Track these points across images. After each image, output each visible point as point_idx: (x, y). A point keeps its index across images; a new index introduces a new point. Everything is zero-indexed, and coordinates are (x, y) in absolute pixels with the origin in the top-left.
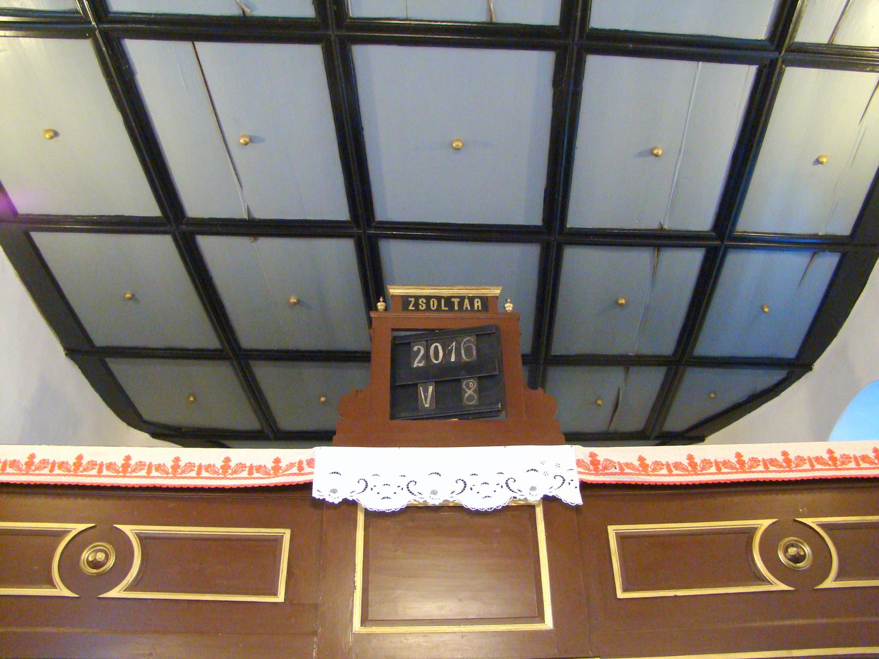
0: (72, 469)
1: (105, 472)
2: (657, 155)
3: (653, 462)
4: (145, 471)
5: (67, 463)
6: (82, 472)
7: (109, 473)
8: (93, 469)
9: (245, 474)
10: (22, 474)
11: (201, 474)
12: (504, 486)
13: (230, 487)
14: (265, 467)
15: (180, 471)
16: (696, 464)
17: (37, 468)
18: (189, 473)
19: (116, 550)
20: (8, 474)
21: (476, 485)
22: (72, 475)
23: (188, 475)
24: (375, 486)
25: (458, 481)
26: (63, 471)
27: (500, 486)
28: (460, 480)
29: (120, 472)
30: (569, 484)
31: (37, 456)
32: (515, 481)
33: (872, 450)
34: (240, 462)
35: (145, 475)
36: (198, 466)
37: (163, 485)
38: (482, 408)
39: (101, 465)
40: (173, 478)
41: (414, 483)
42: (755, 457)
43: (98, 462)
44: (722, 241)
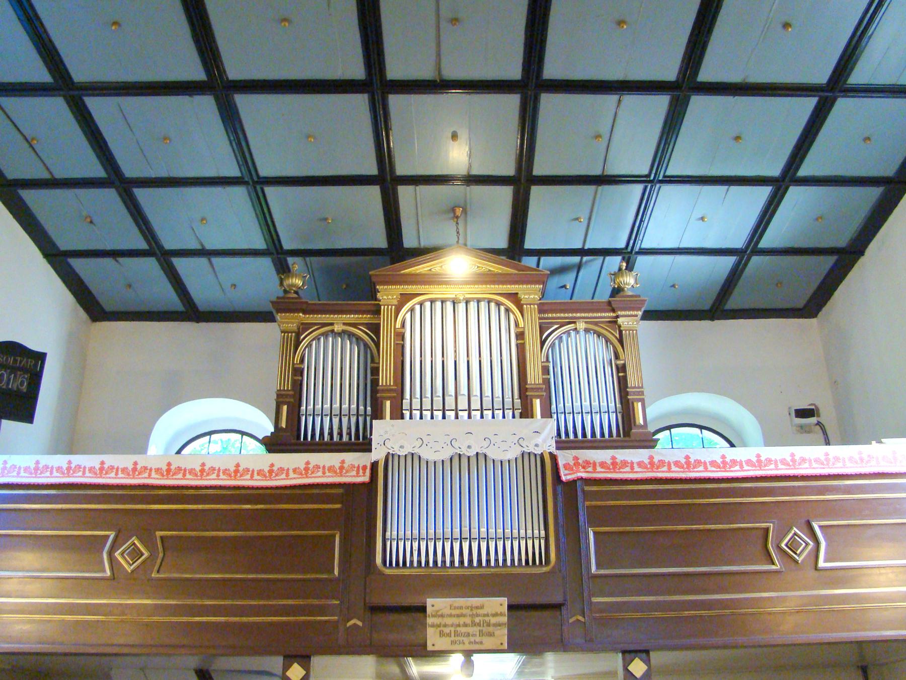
1: (188, 476)
2: (580, 222)
3: (583, 461)
5: (127, 468)
10: (198, 479)
15: (39, 472)
22: (304, 478)
23: (244, 478)
31: (206, 464)
33: (789, 455)
34: (281, 466)
35: (285, 477)
39: (151, 470)
42: (735, 459)
43: (286, 468)
44: (161, 256)
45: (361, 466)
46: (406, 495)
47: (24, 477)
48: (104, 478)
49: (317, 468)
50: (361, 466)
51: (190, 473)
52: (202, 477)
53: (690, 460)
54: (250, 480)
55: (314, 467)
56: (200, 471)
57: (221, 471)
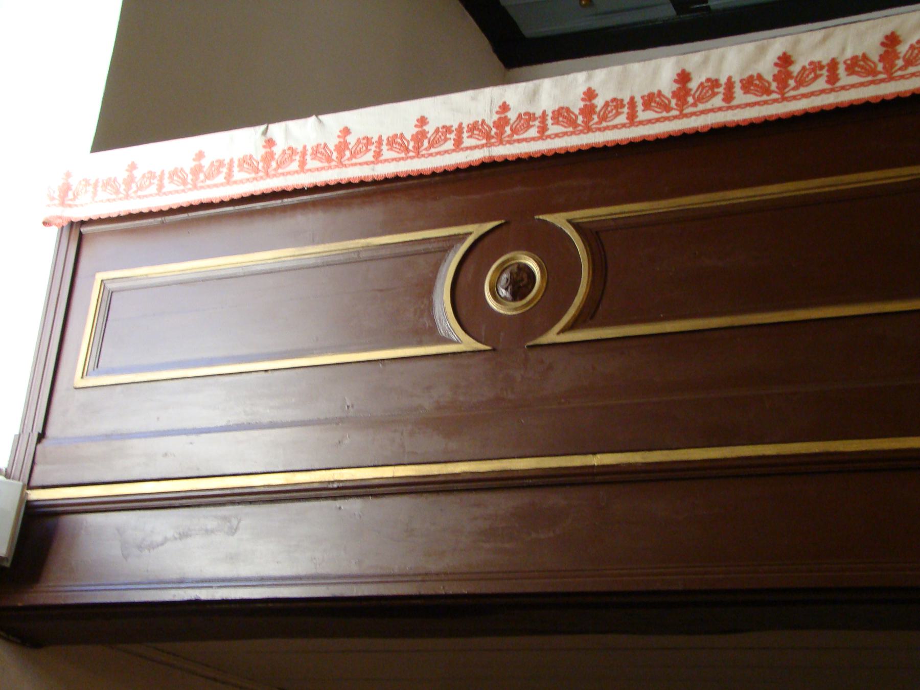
0: (411, 147)
4: (720, 97)
6: (694, 105)
7: (855, 79)
8: (714, 94)
9: (821, 83)
11: (637, 117)
13: (834, 107)
14: (760, 77)
15: (900, 63)
17: (699, 100)
18: (612, 120)
19: (518, 248)
20: (641, 123)
22: (882, 81)
23: (708, 105)
26: (657, 112)
29: (671, 109)
36: (726, 84)
37: (437, 168)
39: (833, 65)
40: (679, 119)
45: (384, 138)
46: (49, 352)
47: (853, 86)
48: (202, 187)
49: (148, 178)
50: (736, 79)
51: (647, 105)
52: (783, 94)
53: (595, 101)
54: (454, 151)
55: (144, 176)
56: (582, 111)
57: (385, 142)
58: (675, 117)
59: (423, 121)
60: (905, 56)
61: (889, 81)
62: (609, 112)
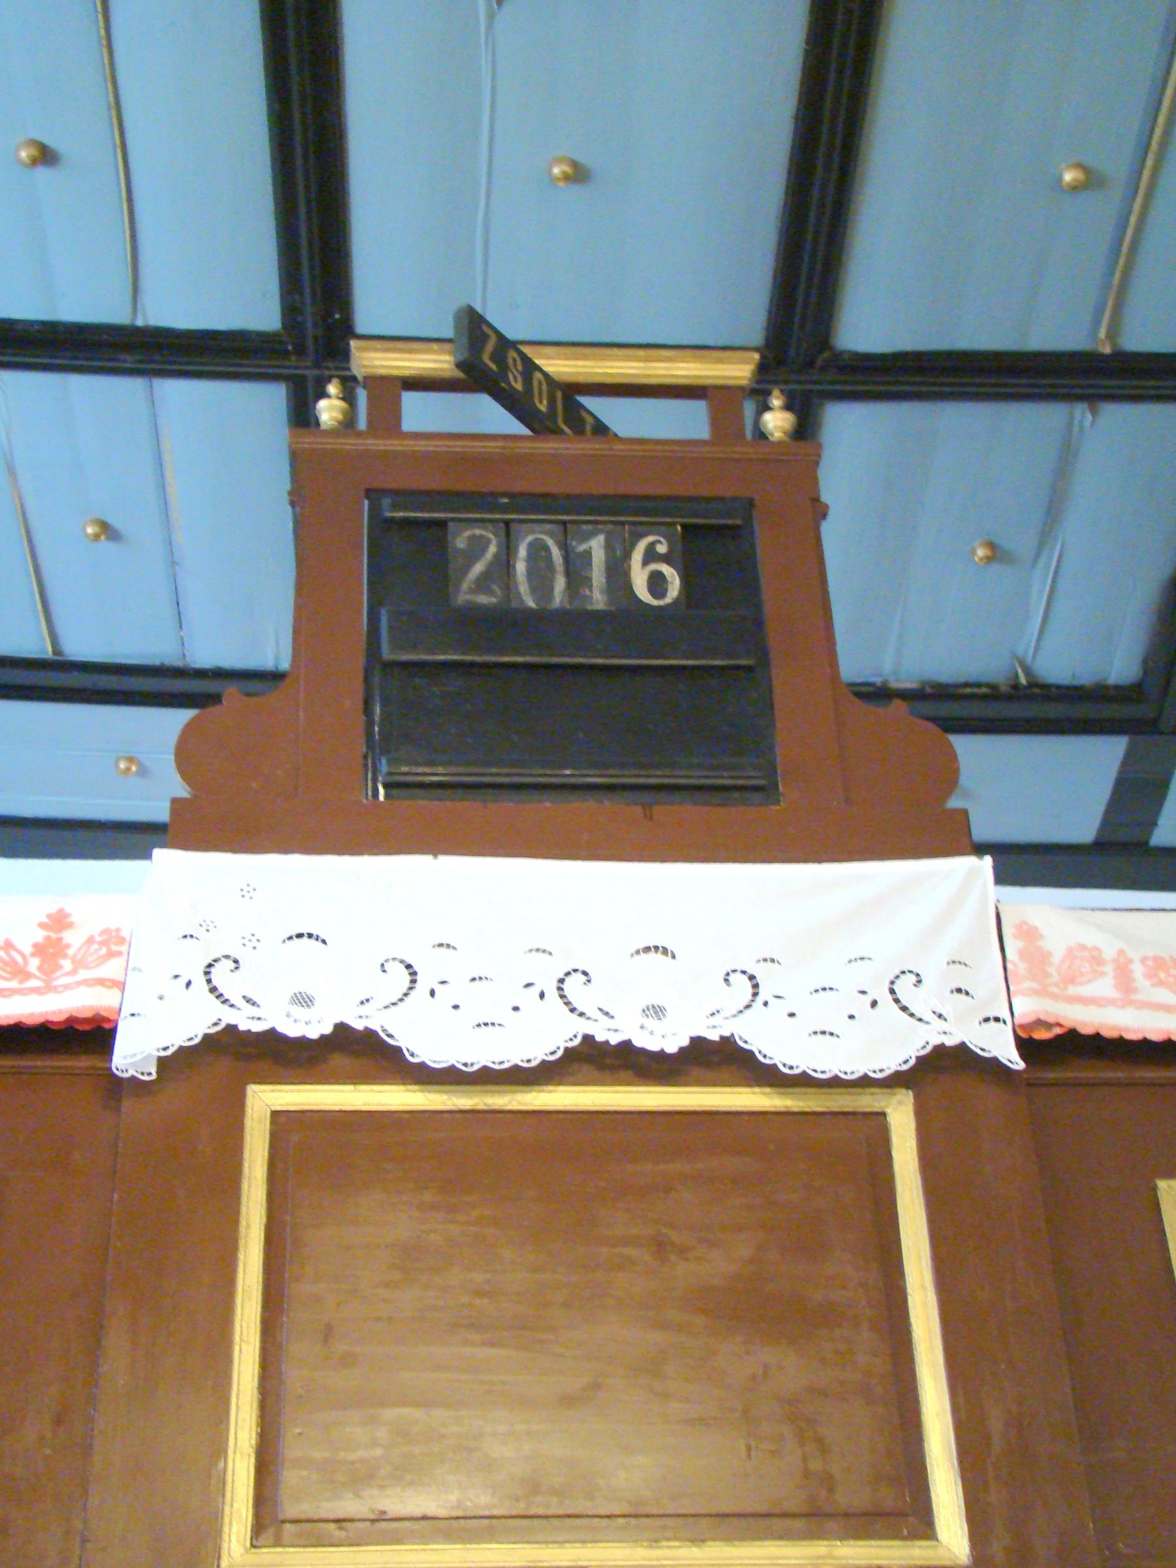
9: (1104, 987)
12: (886, 999)
16: (1045, 956)
21: (809, 994)
24: (443, 982)
25: (734, 978)
27: (535, 991)
28: (734, 971)
29: (29, 976)
30: (432, 993)
32: (919, 982)
38: (534, 772)
41: (913, 978)
58: (36, 991)
59: (59, 921)
60: (75, 955)
61: (1123, 1006)
62: (92, 954)
